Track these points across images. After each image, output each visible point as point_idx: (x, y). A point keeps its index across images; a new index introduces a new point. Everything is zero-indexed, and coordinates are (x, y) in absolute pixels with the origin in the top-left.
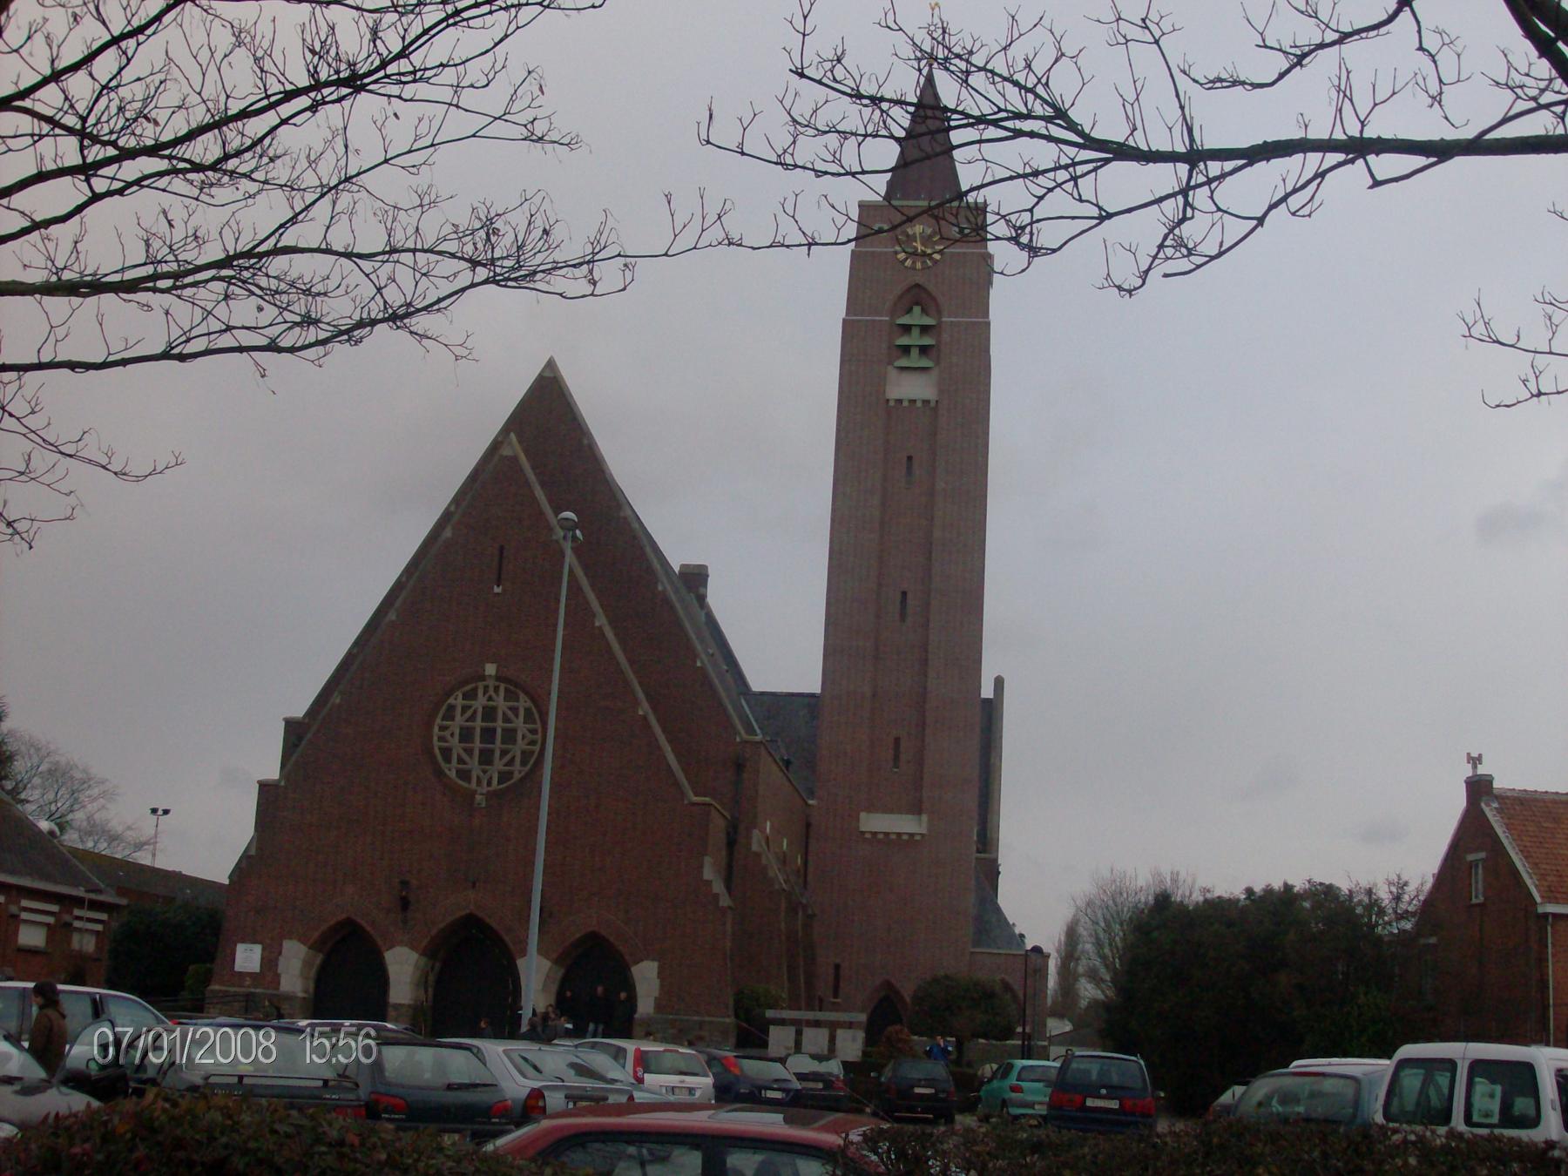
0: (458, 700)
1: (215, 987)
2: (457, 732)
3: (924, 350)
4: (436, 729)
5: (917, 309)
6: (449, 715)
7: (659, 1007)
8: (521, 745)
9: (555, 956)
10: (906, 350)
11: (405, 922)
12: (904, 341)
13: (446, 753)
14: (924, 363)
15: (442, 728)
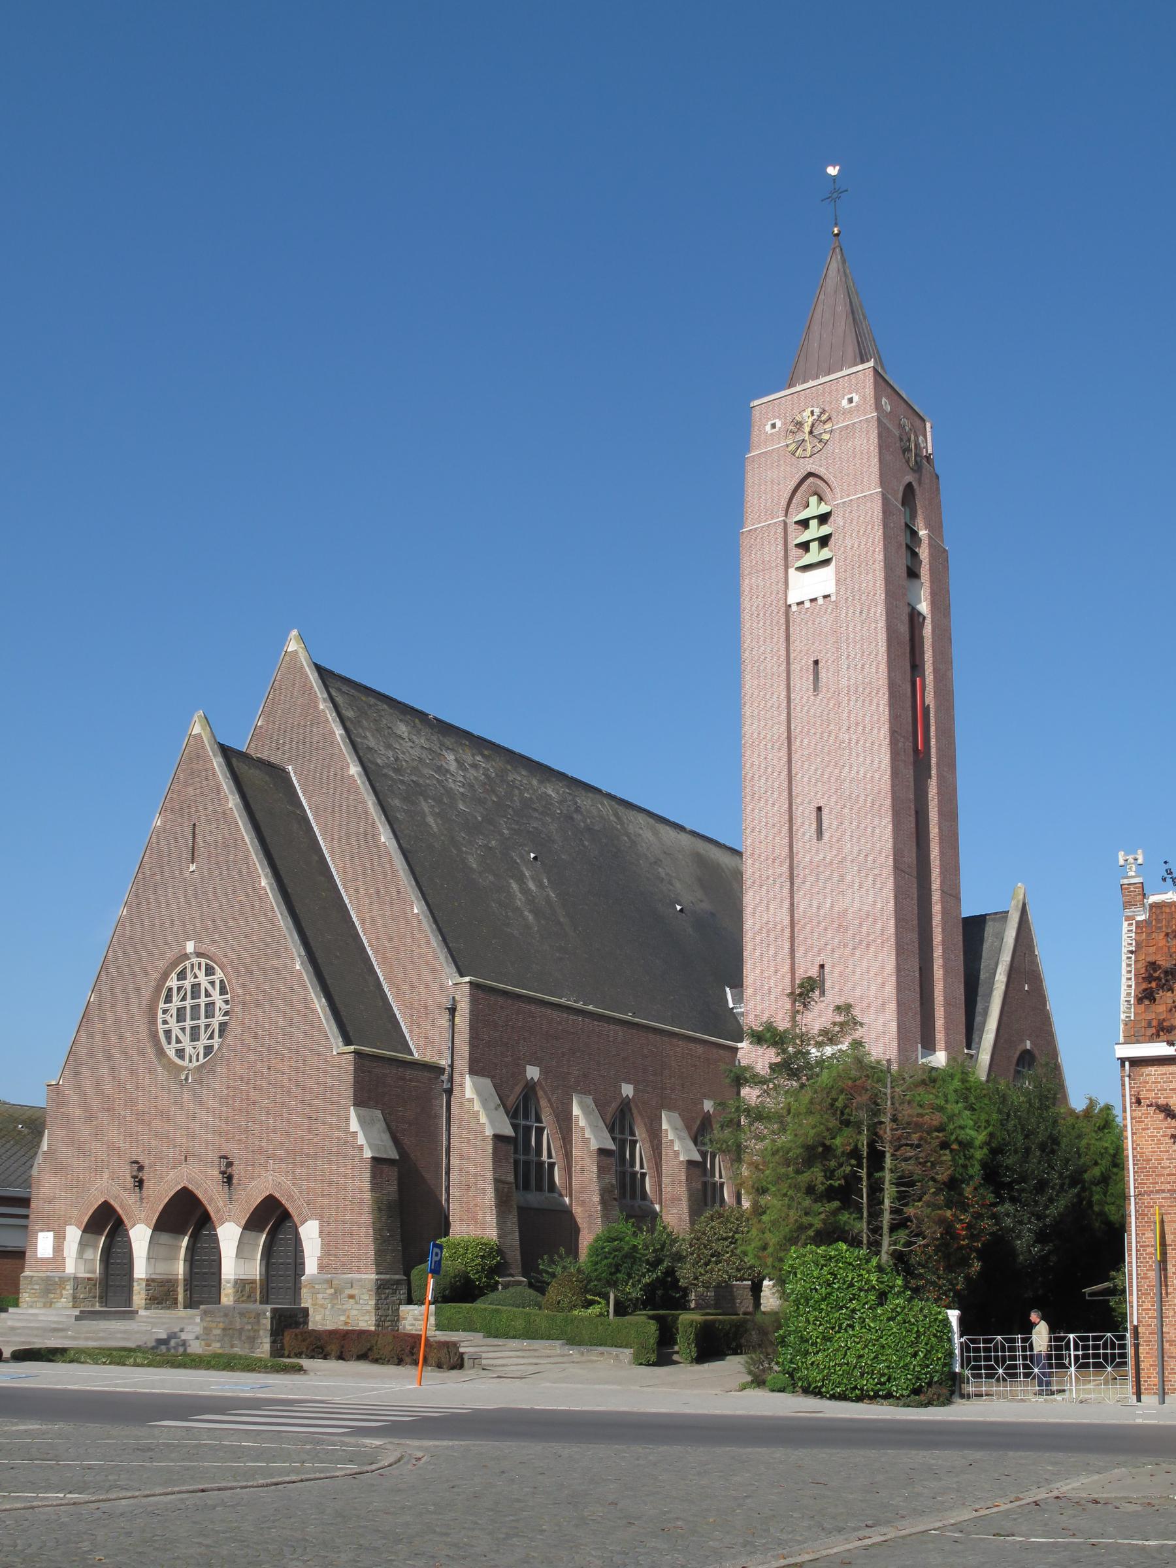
0: (173, 982)
1: (27, 1273)
2: (217, 1012)
3: (824, 541)
4: (160, 1012)
5: (813, 500)
6: (168, 999)
7: (321, 1268)
8: (218, 1018)
9: (243, 1222)
10: (805, 546)
11: (141, 1199)
12: (806, 536)
13: (168, 1033)
14: (826, 553)
15: (165, 1012)
